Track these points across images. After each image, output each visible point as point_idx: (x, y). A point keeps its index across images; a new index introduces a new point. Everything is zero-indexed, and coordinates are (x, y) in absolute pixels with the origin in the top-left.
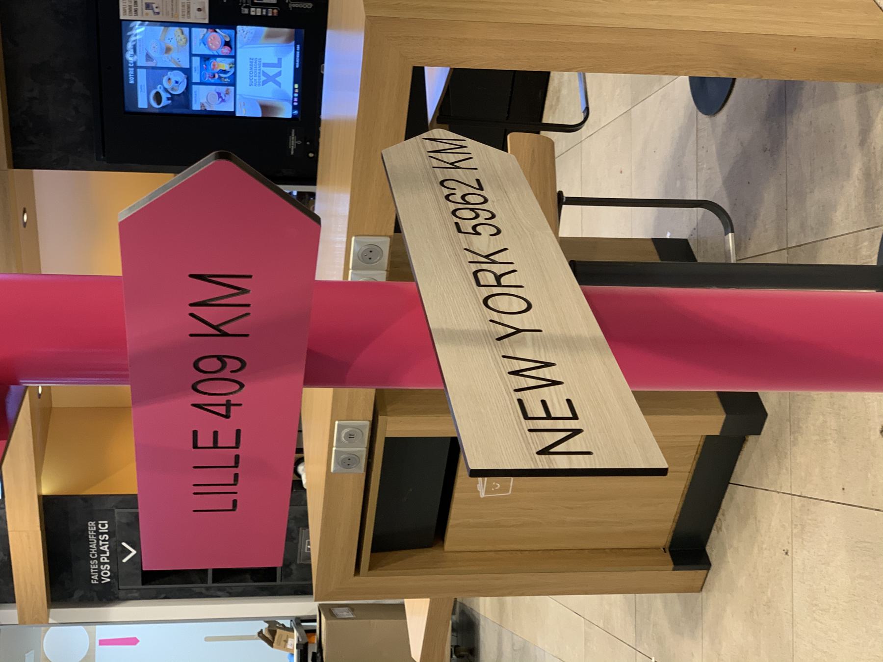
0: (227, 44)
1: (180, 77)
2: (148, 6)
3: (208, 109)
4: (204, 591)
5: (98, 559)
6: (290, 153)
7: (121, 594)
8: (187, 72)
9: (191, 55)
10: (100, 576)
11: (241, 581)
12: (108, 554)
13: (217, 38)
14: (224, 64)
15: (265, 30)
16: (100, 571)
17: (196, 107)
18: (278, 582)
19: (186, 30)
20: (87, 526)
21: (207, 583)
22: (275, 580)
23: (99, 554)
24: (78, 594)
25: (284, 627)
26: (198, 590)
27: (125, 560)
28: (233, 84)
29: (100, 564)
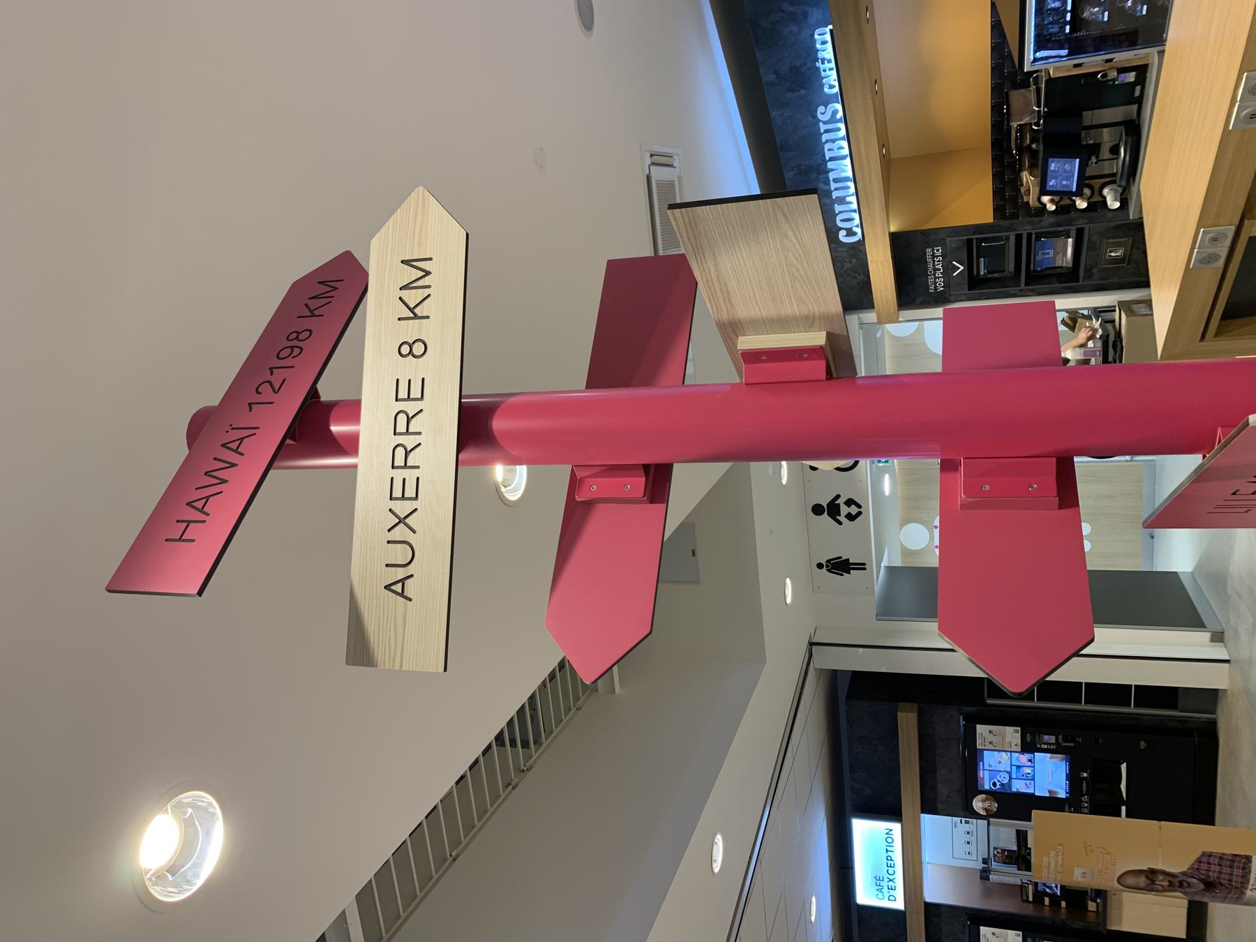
0: (1030, 761)
1: (1007, 776)
2: (991, 743)
3: (1021, 791)
4: (1018, 293)
5: (934, 274)
6: (1063, 737)
7: (952, 298)
8: (1010, 773)
9: (1012, 765)
10: (936, 287)
11: (1048, 284)
12: (942, 271)
13: (1024, 758)
14: (1028, 770)
15: (1049, 755)
16: (935, 283)
17: (1014, 790)
18: (1081, 282)
19: (1009, 754)
20: (926, 252)
21: (1020, 286)
22: (1078, 281)
23: (934, 271)
24: (918, 301)
25: (1084, 316)
26: (1013, 292)
27: (954, 274)
28: (1034, 780)
29: (935, 278)
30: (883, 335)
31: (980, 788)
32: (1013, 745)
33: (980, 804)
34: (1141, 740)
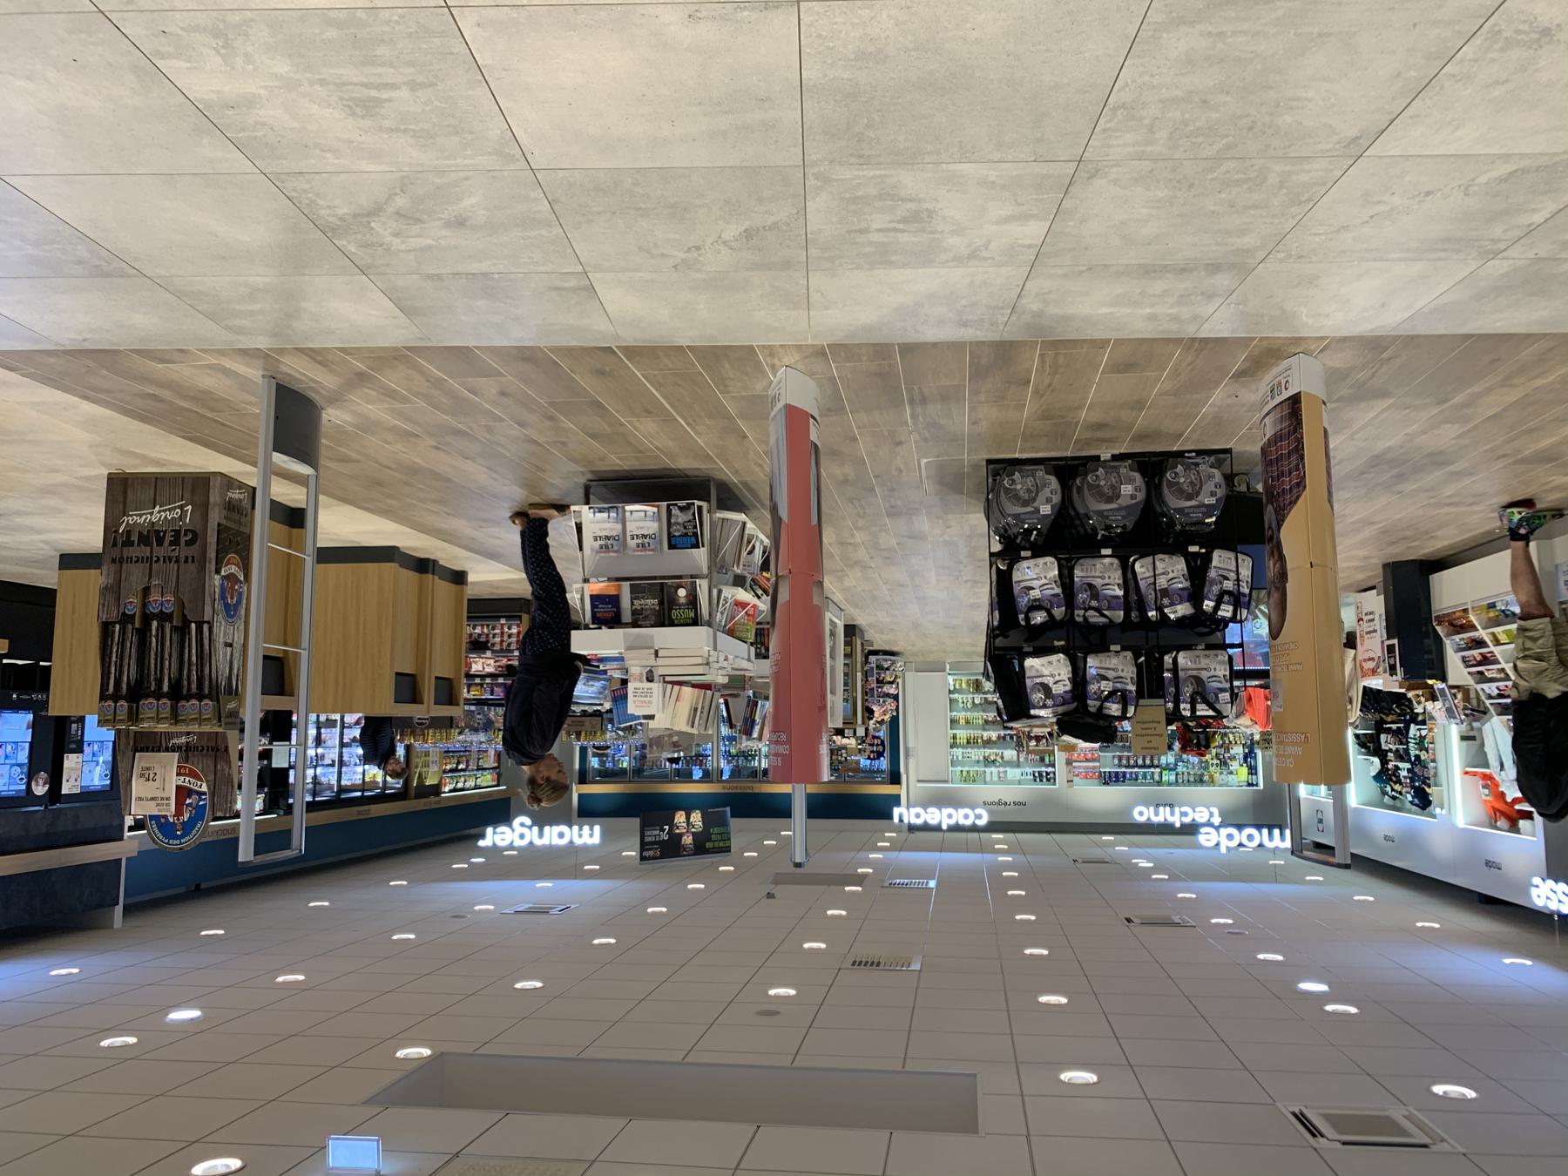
0: (89, 745)
2: (76, 780)
14: (9, 748)
30: (1073, 484)
31: (23, 794)
32: (77, 760)
33: (40, 788)
34: (743, 855)
